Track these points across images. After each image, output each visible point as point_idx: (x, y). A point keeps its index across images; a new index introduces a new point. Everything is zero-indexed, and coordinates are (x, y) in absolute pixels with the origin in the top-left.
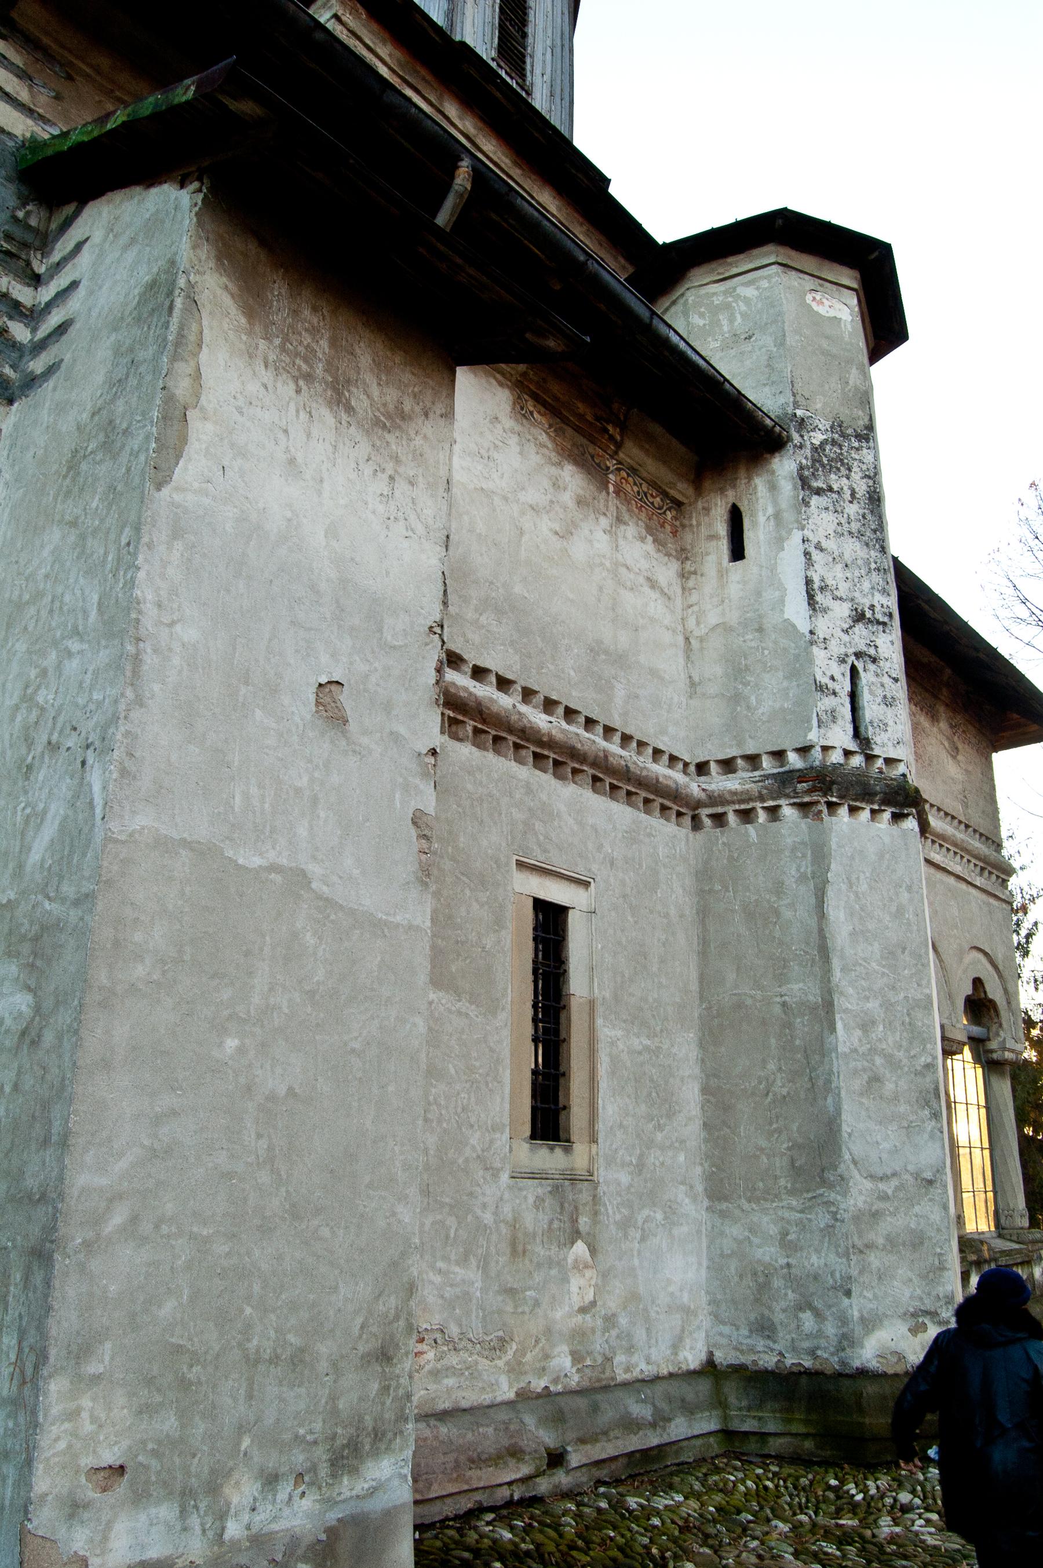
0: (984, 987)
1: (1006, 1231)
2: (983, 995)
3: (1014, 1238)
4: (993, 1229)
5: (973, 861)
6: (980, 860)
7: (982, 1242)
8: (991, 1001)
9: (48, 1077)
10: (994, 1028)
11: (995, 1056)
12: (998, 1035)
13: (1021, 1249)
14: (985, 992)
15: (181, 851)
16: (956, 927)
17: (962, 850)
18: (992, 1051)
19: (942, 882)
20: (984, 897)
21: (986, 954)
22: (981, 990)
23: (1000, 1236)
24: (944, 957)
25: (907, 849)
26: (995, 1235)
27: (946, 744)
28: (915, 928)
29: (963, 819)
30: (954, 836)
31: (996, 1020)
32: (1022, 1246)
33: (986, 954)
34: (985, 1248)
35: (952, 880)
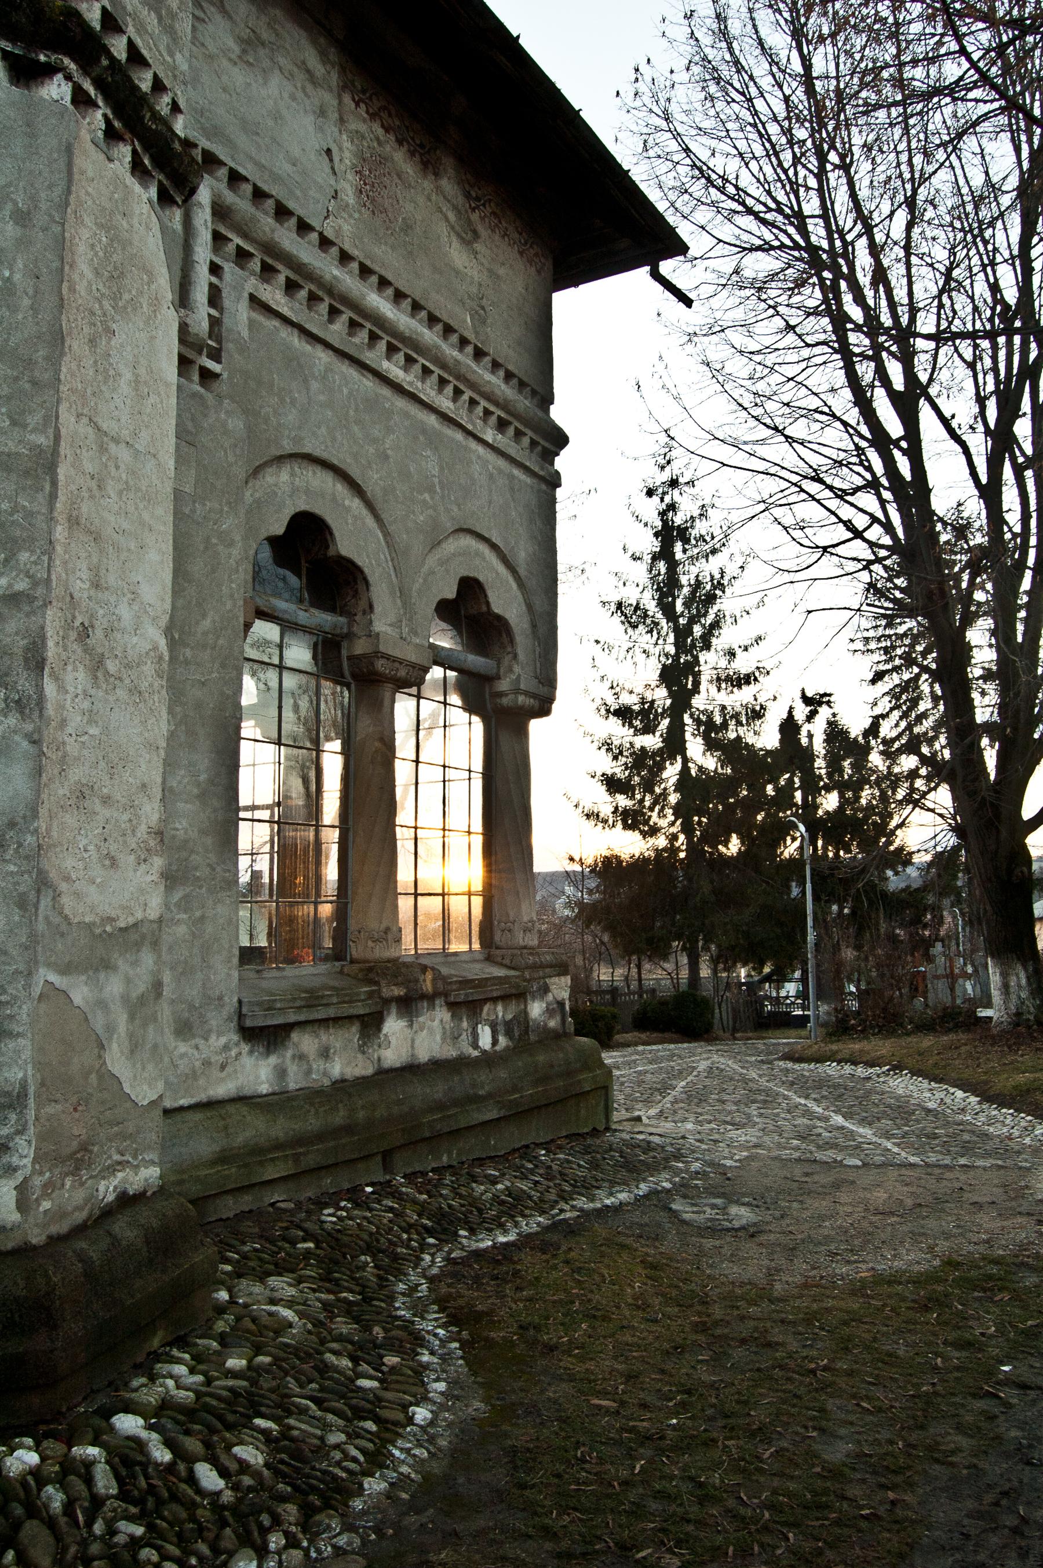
0: (486, 596)
1: (498, 952)
2: (484, 608)
3: (507, 961)
4: (476, 946)
5: (483, 403)
6: (497, 404)
7: (424, 969)
8: (499, 618)
9: (92, 889)
10: (507, 660)
11: (505, 701)
12: (510, 670)
13: (507, 977)
14: (488, 604)
15: (25, 641)
16: (431, 489)
17: (458, 377)
18: (501, 694)
19: (407, 415)
20: (501, 463)
21: (494, 546)
22: (483, 600)
23: (489, 959)
24: (391, 528)
25: (33, 136)
26: (481, 957)
27: (451, 216)
28: (26, 302)
29: (470, 335)
30: (438, 347)
31: (509, 649)
32: (512, 973)
33: (494, 546)
34: (429, 976)
35: (432, 420)
